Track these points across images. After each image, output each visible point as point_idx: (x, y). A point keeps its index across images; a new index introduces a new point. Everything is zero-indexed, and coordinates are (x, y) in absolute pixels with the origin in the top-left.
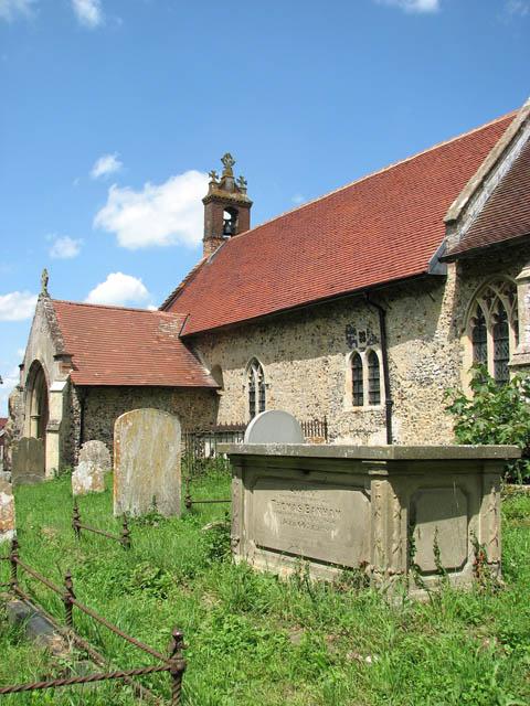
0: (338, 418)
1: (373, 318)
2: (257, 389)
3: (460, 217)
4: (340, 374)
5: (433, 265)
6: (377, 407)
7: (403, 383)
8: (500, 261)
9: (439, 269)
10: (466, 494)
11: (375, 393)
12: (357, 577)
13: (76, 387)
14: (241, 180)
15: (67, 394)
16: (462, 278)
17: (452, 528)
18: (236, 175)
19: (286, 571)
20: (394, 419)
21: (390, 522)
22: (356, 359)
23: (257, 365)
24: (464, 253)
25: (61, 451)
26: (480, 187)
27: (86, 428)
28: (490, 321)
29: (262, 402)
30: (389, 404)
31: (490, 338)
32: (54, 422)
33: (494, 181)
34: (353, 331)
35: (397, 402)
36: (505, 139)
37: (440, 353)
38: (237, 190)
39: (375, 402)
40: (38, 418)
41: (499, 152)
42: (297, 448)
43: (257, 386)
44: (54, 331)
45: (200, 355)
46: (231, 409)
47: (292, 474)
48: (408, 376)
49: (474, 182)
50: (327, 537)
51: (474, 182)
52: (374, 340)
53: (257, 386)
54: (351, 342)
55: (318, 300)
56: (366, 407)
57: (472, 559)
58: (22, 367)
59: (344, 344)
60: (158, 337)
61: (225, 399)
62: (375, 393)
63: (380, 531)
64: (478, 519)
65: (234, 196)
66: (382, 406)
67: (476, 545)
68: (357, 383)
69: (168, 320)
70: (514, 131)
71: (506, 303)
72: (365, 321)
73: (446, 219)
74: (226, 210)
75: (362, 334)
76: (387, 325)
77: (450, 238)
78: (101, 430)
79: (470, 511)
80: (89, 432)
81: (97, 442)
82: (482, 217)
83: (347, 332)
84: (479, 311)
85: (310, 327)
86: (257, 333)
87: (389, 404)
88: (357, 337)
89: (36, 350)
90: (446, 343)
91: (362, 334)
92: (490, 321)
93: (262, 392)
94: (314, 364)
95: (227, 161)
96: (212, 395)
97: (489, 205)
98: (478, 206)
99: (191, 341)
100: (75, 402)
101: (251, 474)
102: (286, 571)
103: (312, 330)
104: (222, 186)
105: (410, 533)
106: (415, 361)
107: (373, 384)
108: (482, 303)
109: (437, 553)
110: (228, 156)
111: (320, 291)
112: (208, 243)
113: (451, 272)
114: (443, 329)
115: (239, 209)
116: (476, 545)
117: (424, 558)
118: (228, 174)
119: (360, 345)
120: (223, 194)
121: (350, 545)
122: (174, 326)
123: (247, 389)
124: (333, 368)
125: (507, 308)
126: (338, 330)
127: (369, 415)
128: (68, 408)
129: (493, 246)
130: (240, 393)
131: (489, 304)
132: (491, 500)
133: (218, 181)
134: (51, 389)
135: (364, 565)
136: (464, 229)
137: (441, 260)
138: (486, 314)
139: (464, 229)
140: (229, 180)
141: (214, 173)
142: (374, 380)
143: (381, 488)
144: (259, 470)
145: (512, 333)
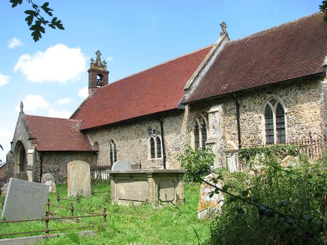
0: (145, 163)
1: (158, 124)
2: (113, 152)
3: (190, 87)
4: (146, 146)
5: (179, 106)
6: (160, 159)
7: (170, 149)
8: (203, 105)
9: (182, 107)
10: (174, 182)
11: (159, 153)
12: (146, 202)
13: (39, 151)
14: (105, 62)
15: (35, 154)
16: (191, 110)
17: (170, 190)
18: (102, 60)
19: (127, 204)
20: (166, 163)
21: (153, 188)
22: (152, 140)
23: (113, 142)
24: (190, 102)
25: (33, 178)
26: (198, 75)
27: (43, 169)
28: (200, 127)
29: (115, 157)
30: (165, 157)
31: (200, 133)
32: (30, 166)
33: (203, 73)
34: (151, 129)
35: (168, 157)
36: (207, 57)
37: (183, 138)
38: (103, 66)
39: (159, 156)
40: (20, 165)
41: (205, 62)
42: (129, 171)
43: (113, 150)
44: (27, 129)
45: (89, 138)
46: (103, 159)
47: (129, 178)
48: (172, 146)
49: (195, 74)
50: (138, 194)
51: (195, 74)
52: (159, 133)
53: (113, 150)
54: (150, 133)
55: (137, 117)
56: (156, 158)
57: (176, 199)
58: (12, 143)
59: (147, 134)
60: (71, 131)
61: (100, 156)
62: (159, 153)
63: (151, 191)
64: (177, 188)
65: (101, 69)
66: (162, 158)
67: (177, 195)
68: (153, 149)
69: (75, 123)
70: (211, 54)
71: (206, 120)
72: (155, 125)
73: (185, 88)
74: (98, 75)
75: (154, 131)
76: (163, 127)
77: (186, 95)
78: (49, 169)
79: (175, 186)
80: (44, 170)
81: (48, 174)
82: (198, 88)
83: (148, 130)
84: (197, 123)
85: (134, 127)
86: (113, 129)
87: (165, 157)
88: (152, 132)
89: (19, 136)
90: (185, 135)
91: (154, 131)
92: (200, 127)
93: (115, 153)
94: (136, 141)
95: (98, 53)
96: (95, 154)
97: (201, 83)
98: (197, 83)
99: (85, 132)
100: (38, 158)
101: (116, 179)
102: (127, 204)
103: (135, 129)
104: (96, 65)
105: (159, 191)
106: (174, 141)
107: (158, 148)
108: (197, 120)
109: (166, 196)
110: (98, 51)
111: (137, 114)
112: (90, 89)
113: (187, 108)
114: (184, 129)
115: (104, 75)
116: (177, 195)
117: (162, 198)
118: (99, 59)
119: (153, 135)
120: (96, 68)
121: (143, 196)
122: (78, 125)
123: (109, 152)
124: (143, 144)
125: (206, 123)
126: (145, 128)
127: (157, 162)
128: (35, 161)
129: (200, 100)
130: (106, 153)
131: (200, 120)
132: (180, 183)
133: (94, 62)
134: (28, 152)
135: (147, 200)
136: (191, 92)
137: (182, 104)
138: (199, 124)
139: (191, 92)
140: (99, 62)
141: (92, 59)
142: (159, 148)
143: (151, 180)
144: (118, 177)
145: (207, 130)
